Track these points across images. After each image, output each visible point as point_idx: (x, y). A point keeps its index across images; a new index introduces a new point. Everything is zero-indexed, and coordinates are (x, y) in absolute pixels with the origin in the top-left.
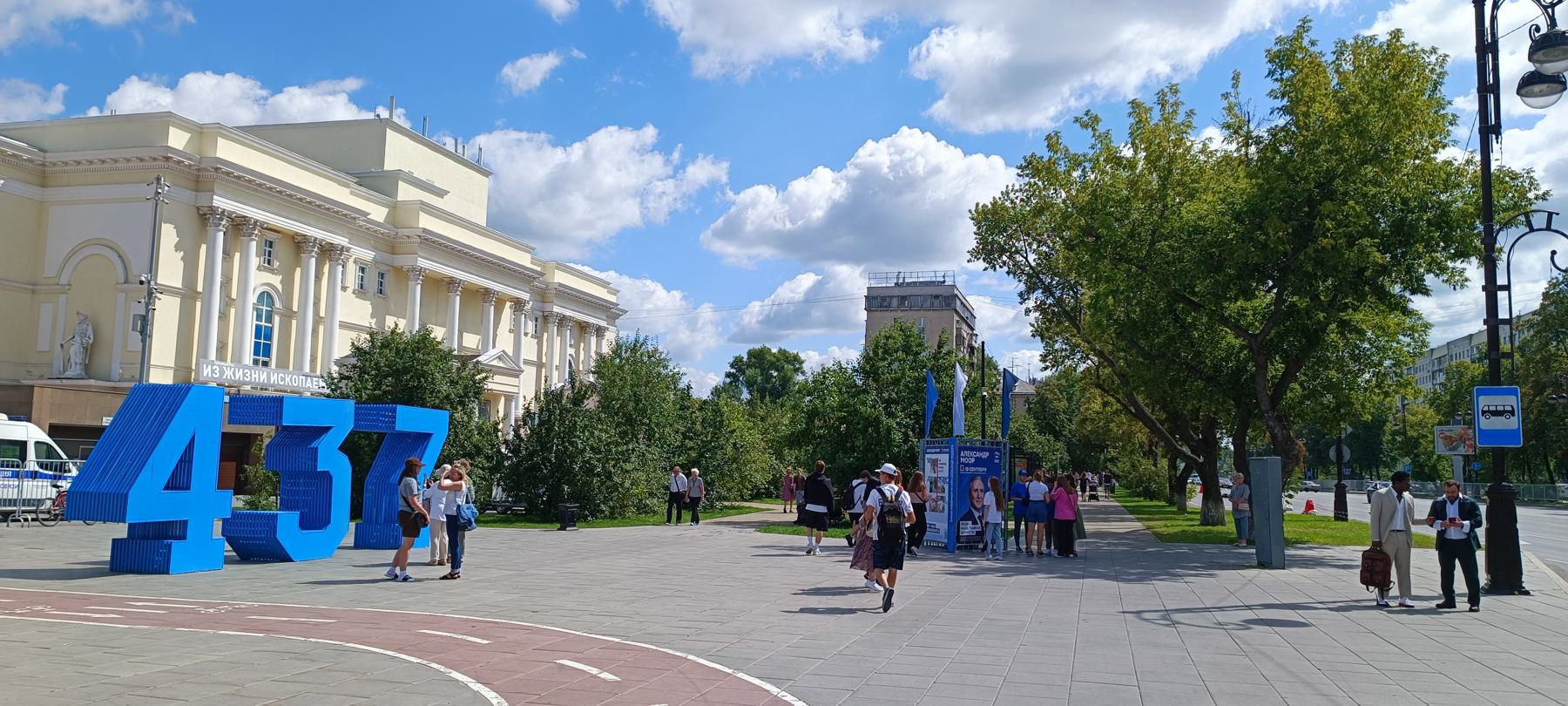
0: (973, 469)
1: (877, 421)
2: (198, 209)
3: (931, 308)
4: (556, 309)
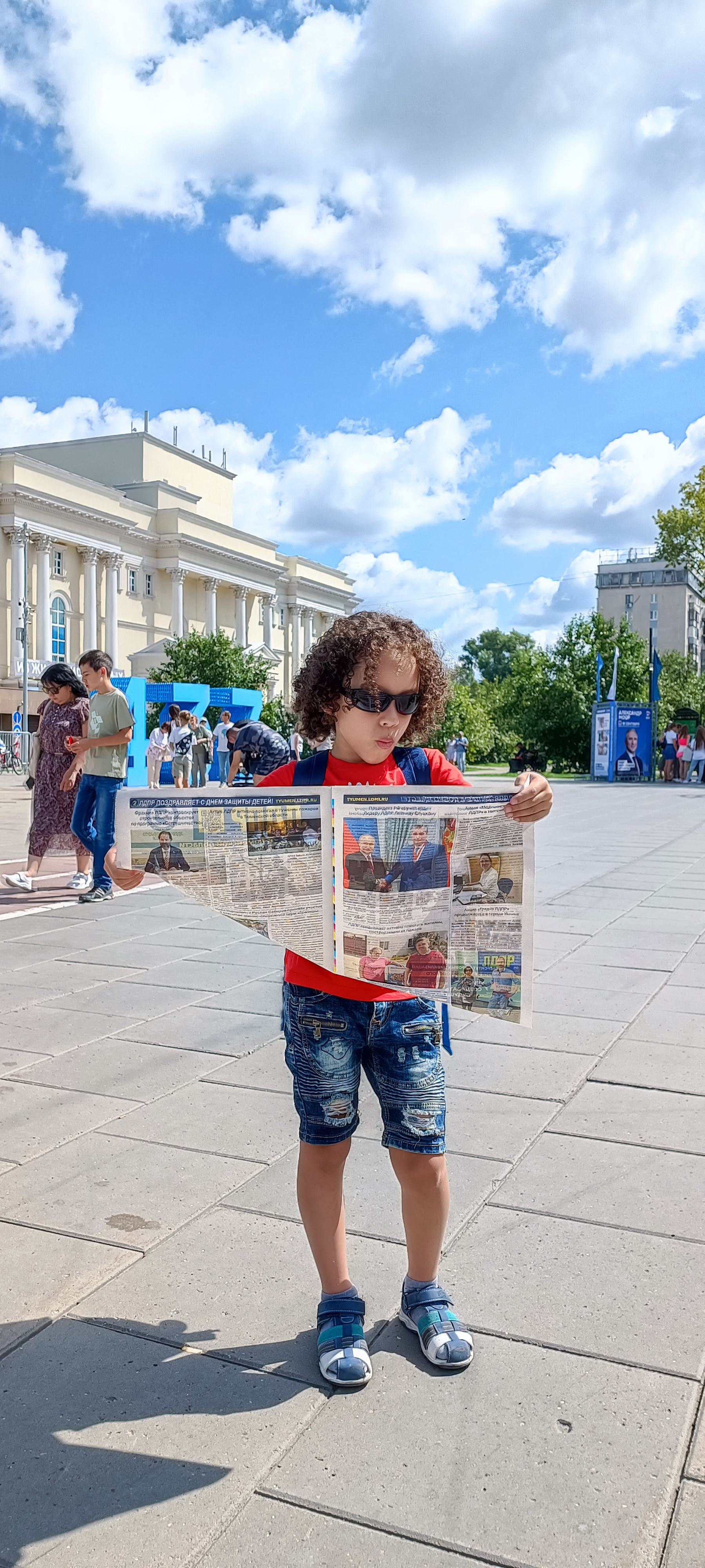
0: (628, 724)
1: (571, 693)
2: (3, 529)
3: (663, 584)
4: (299, 602)
